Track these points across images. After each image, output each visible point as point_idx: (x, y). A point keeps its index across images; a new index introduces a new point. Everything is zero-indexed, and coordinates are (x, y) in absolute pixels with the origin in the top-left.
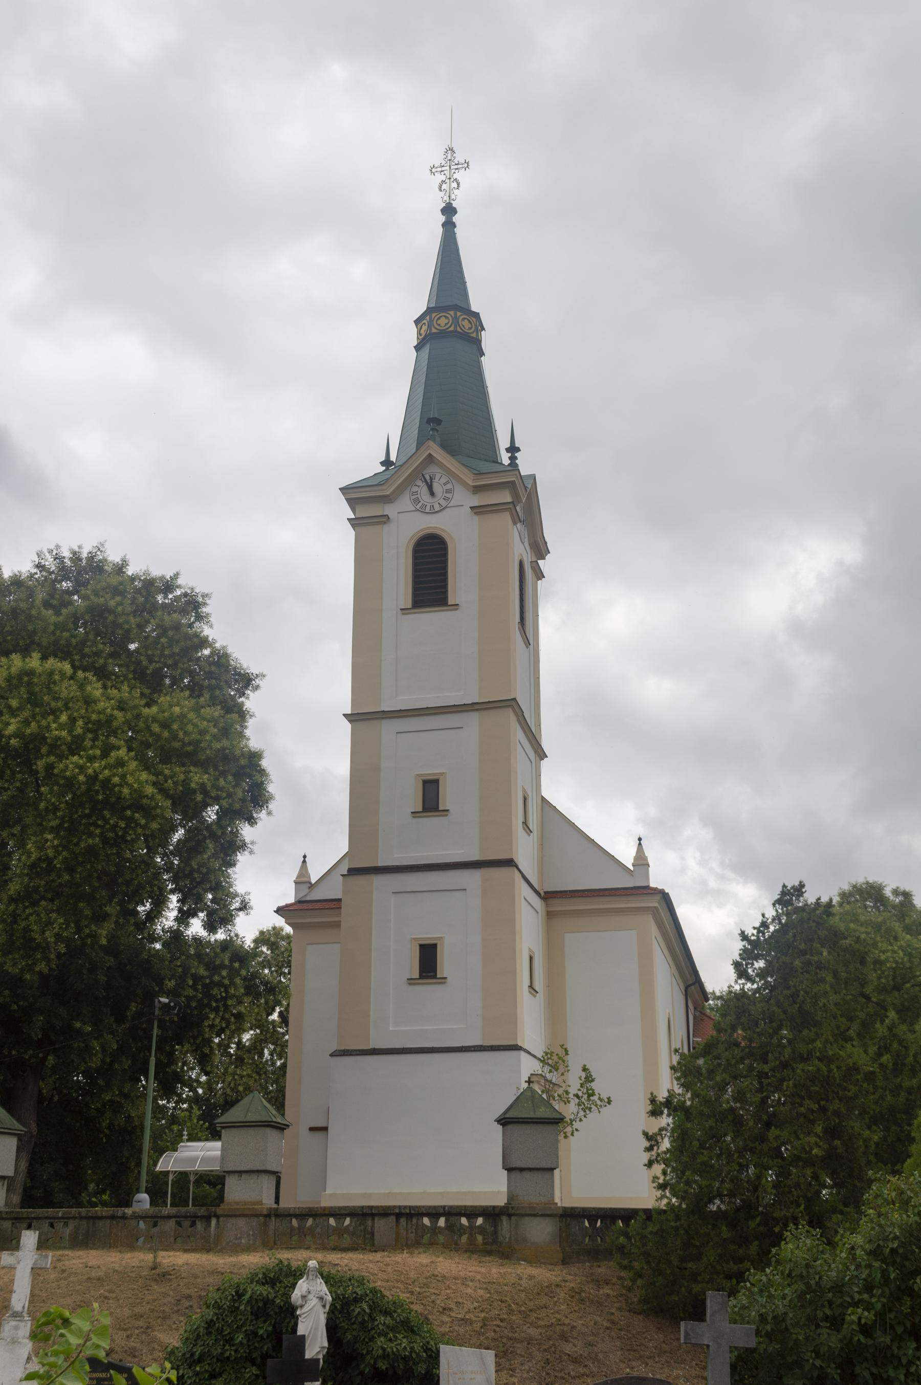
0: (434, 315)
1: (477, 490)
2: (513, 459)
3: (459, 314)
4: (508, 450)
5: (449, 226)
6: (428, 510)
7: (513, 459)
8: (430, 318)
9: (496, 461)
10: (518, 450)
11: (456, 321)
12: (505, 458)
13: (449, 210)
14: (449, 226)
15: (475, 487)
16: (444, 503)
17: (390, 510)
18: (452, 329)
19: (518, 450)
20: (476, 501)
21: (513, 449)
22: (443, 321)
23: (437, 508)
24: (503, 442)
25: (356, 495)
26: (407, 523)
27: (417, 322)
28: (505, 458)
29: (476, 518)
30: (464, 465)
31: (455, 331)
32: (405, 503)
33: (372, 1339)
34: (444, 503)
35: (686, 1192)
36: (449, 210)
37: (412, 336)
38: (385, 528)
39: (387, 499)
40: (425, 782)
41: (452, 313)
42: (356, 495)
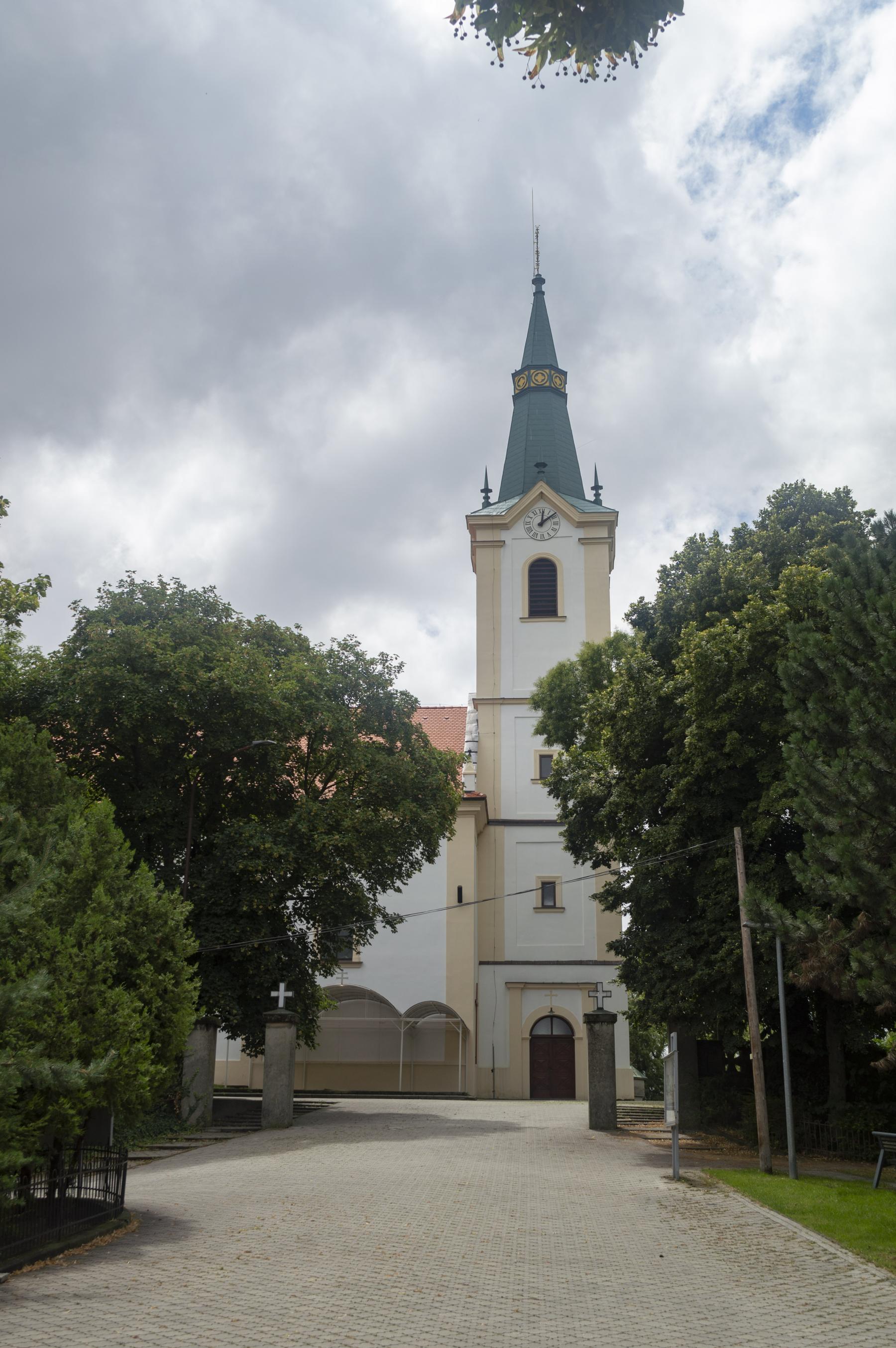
0: (532, 371)
1: (581, 525)
2: (597, 495)
3: (553, 372)
4: (592, 488)
5: (539, 295)
6: (539, 538)
7: (597, 495)
8: (529, 373)
9: (581, 495)
10: (601, 488)
11: (550, 377)
12: (590, 495)
13: (538, 281)
14: (539, 295)
15: (578, 522)
16: (552, 533)
17: (504, 536)
18: (547, 384)
19: (601, 488)
20: (581, 533)
21: (597, 488)
22: (540, 378)
23: (546, 537)
24: (587, 483)
25: (467, 516)
26: (520, 550)
27: (514, 375)
28: (590, 495)
29: (582, 548)
30: (572, 505)
31: (550, 387)
32: (519, 530)
33: (137, 720)
34: (552, 533)
35: (343, 735)
36: (538, 281)
37: (508, 389)
38: (502, 549)
39: (505, 527)
40: (542, 757)
41: (547, 371)
42: (467, 516)
